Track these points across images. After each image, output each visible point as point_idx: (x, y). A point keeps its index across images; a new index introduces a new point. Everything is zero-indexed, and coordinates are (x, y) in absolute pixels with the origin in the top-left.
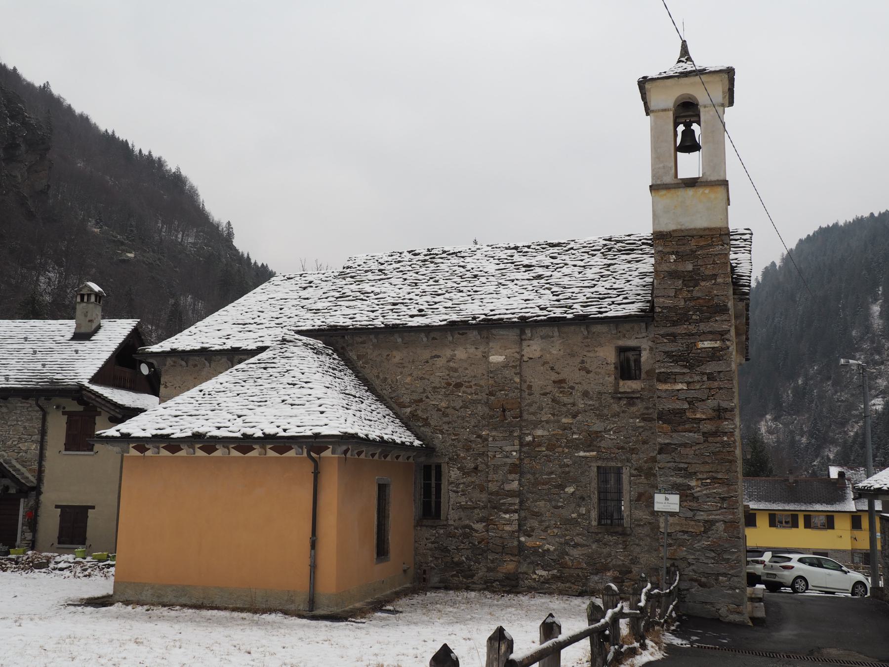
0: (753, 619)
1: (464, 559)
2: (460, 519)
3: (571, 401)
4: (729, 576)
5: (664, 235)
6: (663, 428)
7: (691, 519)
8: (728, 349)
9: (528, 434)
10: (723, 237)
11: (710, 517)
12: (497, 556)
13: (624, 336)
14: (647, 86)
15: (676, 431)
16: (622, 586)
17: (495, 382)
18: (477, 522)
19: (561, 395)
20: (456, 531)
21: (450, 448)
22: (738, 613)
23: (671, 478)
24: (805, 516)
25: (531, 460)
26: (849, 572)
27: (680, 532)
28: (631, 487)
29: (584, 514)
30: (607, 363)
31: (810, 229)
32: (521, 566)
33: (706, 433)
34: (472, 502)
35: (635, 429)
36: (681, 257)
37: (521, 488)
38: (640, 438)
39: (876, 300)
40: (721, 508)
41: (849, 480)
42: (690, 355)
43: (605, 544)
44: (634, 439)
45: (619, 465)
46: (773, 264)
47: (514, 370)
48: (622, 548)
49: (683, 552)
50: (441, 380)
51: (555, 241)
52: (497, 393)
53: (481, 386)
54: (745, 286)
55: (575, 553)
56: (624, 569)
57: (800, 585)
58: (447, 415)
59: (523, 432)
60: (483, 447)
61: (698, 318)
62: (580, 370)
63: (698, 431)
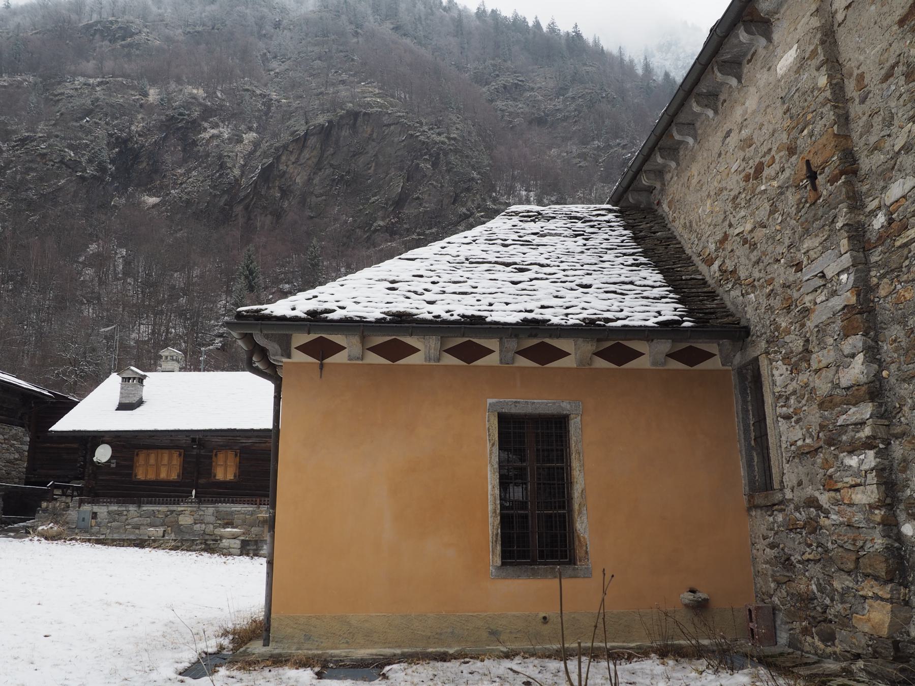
20: (798, 515)
52: (798, 142)
59: (868, 210)
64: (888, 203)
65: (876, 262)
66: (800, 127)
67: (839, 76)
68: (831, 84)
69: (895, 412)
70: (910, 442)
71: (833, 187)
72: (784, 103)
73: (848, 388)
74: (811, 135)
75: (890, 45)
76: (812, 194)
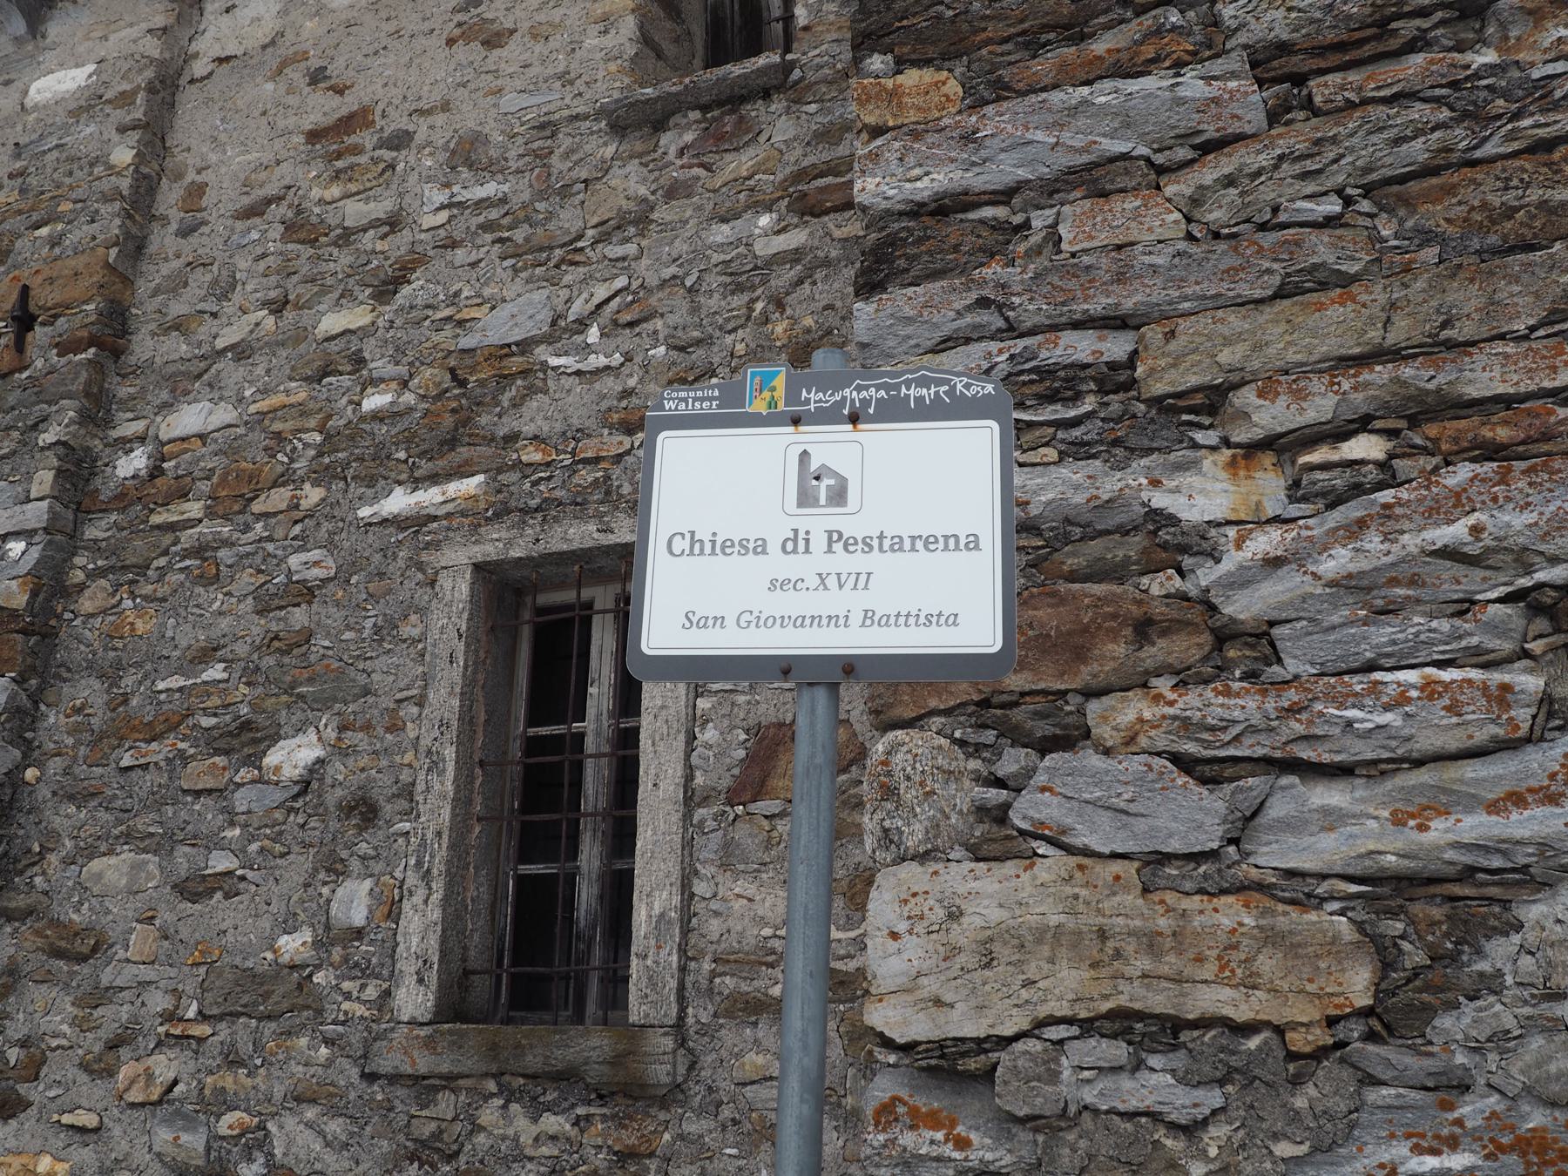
6: (895, 94)
11: (1440, 831)
15: (1002, 91)
19: (335, 191)
25: (117, 587)
27: (1088, 1027)
29: (359, 933)
33: (1283, 48)
38: (779, 329)
47: (119, 115)
52: (19, 244)
59: (115, 434)
64: (164, 436)
65: (95, 541)
66: (35, 217)
67: (157, 167)
68: (136, 171)
69: (24, 862)
70: (38, 933)
71: (64, 360)
72: (18, 156)
74: (55, 242)
75: (278, 163)
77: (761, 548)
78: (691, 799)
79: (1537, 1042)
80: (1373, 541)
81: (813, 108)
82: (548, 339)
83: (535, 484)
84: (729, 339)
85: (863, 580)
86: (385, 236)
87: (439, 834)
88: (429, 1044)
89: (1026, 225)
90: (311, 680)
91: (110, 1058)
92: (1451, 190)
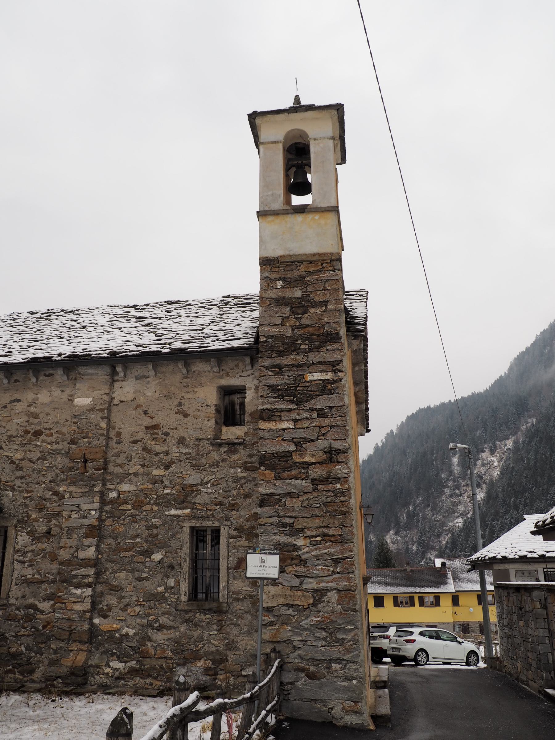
0: (375, 718)
1: (23, 648)
2: (24, 597)
3: (164, 449)
4: (344, 662)
5: (271, 260)
6: (265, 474)
7: (298, 588)
8: (341, 381)
9: (112, 489)
10: (335, 263)
11: (321, 585)
12: (62, 644)
13: (228, 375)
14: (258, 121)
16: (215, 679)
17: (78, 428)
18: (44, 600)
19: (153, 443)
20: (17, 612)
21: (21, 508)
22: (356, 712)
23: (274, 537)
24: (419, 597)
25: (114, 521)
26: (463, 642)
27: (284, 605)
28: (229, 552)
29: (173, 588)
30: (207, 405)
31: (413, 410)
32: (92, 657)
33: (315, 479)
34: (40, 574)
35: (236, 480)
36: (289, 283)
37: (100, 556)
38: (242, 491)
39: (455, 454)
40: (334, 573)
41: (449, 568)
42: (298, 388)
43: (196, 625)
44: (235, 492)
45: (216, 524)
46: (392, 431)
47: (100, 414)
48: (216, 630)
49: (286, 632)
50: (18, 427)
51: (174, 299)
53: (64, 434)
54: (360, 324)
55: (160, 637)
56: (218, 657)
57: (422, 658)
58: (21, 469)
59: (107, 487)
60: (59, 506)
61: (307, 347)
62: (176, 413)
63: (307, 477)
71: (97, 472)
73: (81, 560)
74: (90, 443)
75: (139, 432)
76: (83, 469)
77: (257, 567)
78: (228, 569)
79: (327, 607)
80: (318, 551)
81: (248, 450)
82: (201, 485)
83: (200, 513)
84: (233, 491)
85: (266, 570)
86: (165, 456)
87: (186, 572)
88: (187, 605)
89: (282, 500)
90: (159, 543)
91: (126, 608)
92: (332, 506)
